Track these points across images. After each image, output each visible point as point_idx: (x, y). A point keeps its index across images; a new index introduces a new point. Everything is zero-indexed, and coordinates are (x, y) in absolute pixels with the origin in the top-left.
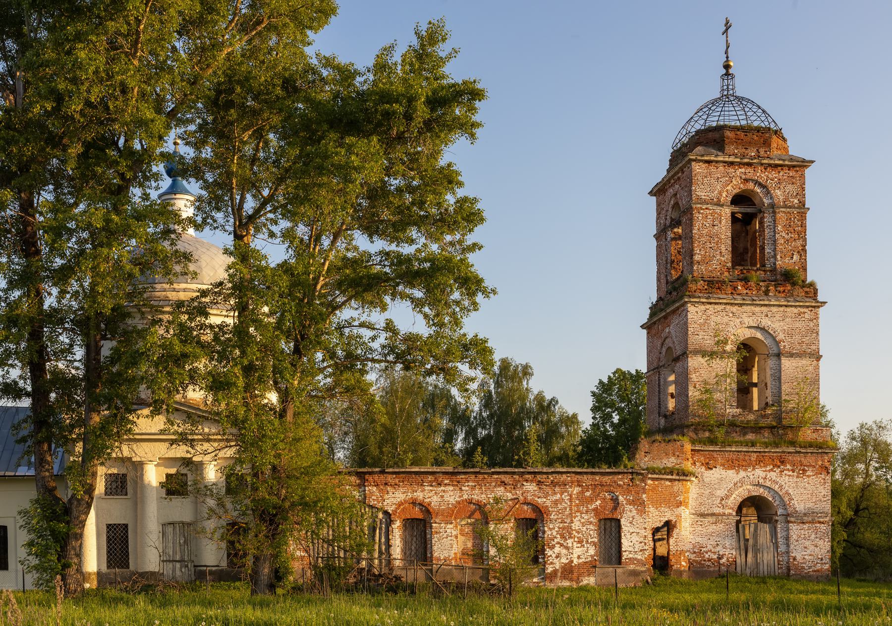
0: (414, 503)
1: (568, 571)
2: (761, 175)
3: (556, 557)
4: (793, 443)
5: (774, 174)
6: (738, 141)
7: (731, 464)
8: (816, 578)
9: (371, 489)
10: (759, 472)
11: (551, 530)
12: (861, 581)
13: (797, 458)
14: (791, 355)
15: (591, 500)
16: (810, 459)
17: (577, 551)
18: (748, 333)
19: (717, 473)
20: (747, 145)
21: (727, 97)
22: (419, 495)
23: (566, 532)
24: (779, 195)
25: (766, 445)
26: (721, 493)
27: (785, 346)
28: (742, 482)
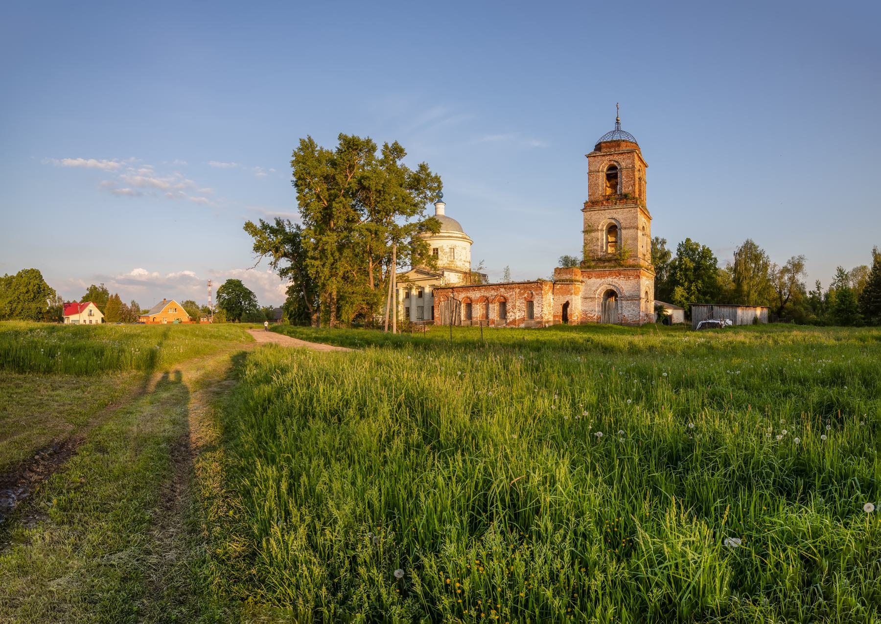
0: (468, 297)
1: (514, 321)
2: (616, 158)
3: (510, 317)
4: (622, 266)
5: (621, 156)
6: (607, 147)
7: (599, 276)
8: (270, 316)
9: (455, 293)
10: (610, 279)
11: (509, 306)
12: (130, 315)
13: (626, 272)
14: (625, 228)
15: (523, 294)
16: (631, 272)
17: (518, 314)
18: (609, 221)
19: (593, 280)
20: (610, 148)
21: (618, 130)
22: (469, 295)
23: (514, 307)
24: (623, 164)
25: (611, 267)
26: (594, 289)
27: (623, 225)
28: (603, 284)
